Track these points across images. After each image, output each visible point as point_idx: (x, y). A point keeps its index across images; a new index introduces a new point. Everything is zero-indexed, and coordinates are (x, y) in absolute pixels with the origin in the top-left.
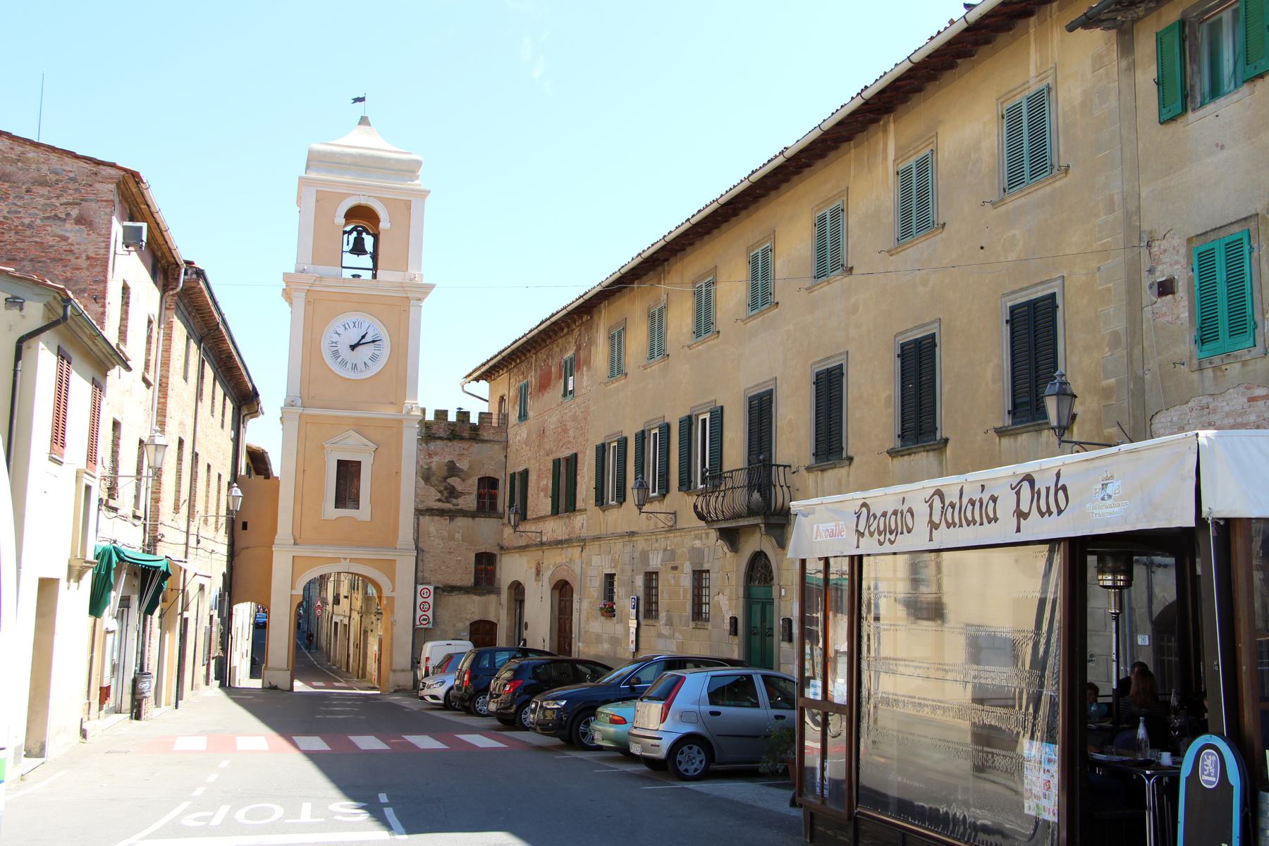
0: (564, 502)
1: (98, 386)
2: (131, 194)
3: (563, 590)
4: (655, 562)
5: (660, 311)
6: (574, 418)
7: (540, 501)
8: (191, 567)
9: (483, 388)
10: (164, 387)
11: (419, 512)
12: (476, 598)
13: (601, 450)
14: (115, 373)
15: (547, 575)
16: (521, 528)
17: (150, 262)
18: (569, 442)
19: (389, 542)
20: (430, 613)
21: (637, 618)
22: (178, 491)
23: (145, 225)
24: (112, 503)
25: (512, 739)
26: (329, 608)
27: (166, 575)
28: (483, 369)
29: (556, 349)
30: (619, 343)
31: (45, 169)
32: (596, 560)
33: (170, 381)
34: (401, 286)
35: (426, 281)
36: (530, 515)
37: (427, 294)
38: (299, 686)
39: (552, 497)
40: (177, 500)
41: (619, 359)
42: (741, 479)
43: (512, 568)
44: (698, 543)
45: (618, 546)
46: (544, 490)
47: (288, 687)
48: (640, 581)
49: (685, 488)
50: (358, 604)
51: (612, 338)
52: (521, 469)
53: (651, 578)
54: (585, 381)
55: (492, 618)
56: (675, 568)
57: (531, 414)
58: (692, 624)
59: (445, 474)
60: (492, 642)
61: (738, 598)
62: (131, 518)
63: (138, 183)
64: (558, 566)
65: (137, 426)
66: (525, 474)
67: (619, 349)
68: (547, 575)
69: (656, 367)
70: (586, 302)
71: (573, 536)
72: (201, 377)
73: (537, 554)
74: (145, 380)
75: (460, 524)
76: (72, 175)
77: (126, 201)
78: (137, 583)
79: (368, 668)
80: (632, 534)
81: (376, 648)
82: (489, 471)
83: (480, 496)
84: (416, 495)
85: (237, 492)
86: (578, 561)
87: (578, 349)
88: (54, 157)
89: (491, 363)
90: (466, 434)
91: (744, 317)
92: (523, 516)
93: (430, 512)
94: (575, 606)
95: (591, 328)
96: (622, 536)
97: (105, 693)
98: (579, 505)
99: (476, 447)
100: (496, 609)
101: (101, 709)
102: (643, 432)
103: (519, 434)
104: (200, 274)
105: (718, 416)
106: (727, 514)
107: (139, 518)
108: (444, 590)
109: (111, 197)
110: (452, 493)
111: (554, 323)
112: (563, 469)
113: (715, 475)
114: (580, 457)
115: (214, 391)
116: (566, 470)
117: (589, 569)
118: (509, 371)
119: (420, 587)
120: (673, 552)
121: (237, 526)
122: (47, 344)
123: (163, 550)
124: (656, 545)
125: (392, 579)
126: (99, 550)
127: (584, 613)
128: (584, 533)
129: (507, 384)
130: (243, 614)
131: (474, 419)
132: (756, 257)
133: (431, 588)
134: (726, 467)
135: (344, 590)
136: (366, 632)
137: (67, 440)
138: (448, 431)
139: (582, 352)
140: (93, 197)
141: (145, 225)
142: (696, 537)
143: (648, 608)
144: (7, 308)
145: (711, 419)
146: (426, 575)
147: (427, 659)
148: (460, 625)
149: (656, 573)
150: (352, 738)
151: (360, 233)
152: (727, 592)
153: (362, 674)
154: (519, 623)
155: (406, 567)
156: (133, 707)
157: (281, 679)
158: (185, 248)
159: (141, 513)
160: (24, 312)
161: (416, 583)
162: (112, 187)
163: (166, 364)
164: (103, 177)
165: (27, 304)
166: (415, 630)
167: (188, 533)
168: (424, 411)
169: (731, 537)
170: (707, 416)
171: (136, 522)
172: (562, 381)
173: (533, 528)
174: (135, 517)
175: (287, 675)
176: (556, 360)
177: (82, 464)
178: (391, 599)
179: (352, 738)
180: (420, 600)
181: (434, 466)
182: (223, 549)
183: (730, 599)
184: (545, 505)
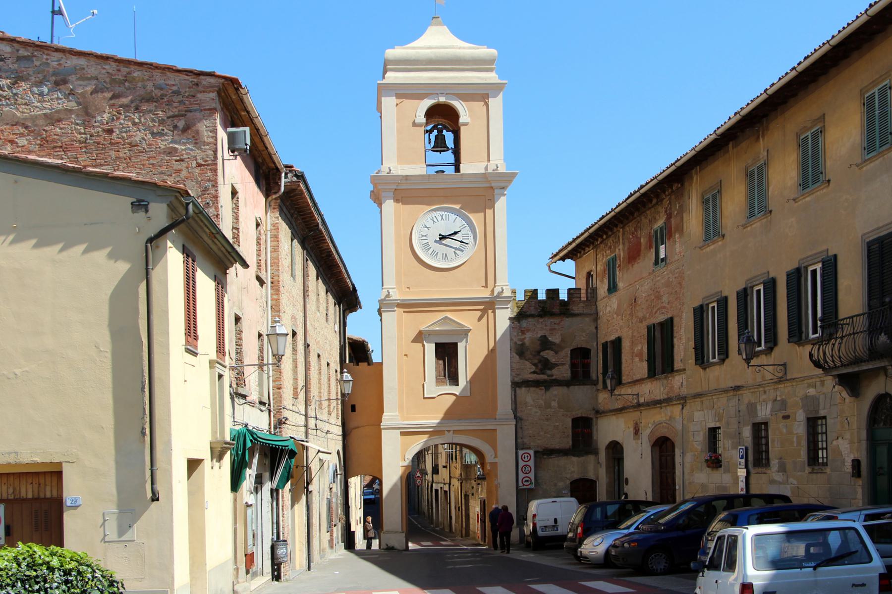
0: (661, 361)
1: (221, 283)
2: (232, 103)
3: (663, 448)
4: (764, 412)
5: (760, 169)
6: (668, 284)
7: (634, 364)
8: (313, 445)
9: (569, 266)
10: (276, 286)
11: (516, 385)
12: (575, 459)
13: (700, 312)
14: (235, 272)
15: (646, 433)
16: (616, 392)
17: (253, 170)
18: (664, 307)
19: (490, 413)
20: (532, 475)
21: (746, 467)
22: (296, 379)
23: (247, 129)
24: (241, 391)
25: (640, 584)
26: (429, 477)
27: (292, 454)
28: (570, 248)
29: (645, 221)
30: (714, 206)
31: (150, 85)
32: (698, 415)
33: (281, 279)
34: (485, 176)
36: (625, 379)
37: (510, 181)
38: (411, 546)
39: (648, 361)
40: (295, 389)
41: (715, 221)
42: (861, 324)
43: (611, 429)
44: (812, 391)
45: (722, 401)
46: (640, 355)
47: (404, 547)
48: (747, 432)
49: (795, 339)
50: (457, 472)
51: (705, 202)
52: (613, 338)
53: (760, 430)
54: (678, 248)
55: (591, 476)
56: (786, 417)
57: (621, 285)
58: (808, 469)
60: (593, 497)
61: (860, 441)
62: (257, 405)
63: (237, 89)
64: (658, 425)
65: (256, 320)
66: (617, 343)
67: (714, 212)
68: (646, 433)
69: (757, 225)
70: (678, 168)
71: (671, 395)
72: (305, 276)
73: (634, 415)
74: (259, 279)
75: (555, 393)
76: (175, 88)
77: (228, 109)
78: (267, 462)
79: (471, 527)
80: (737, 388)
81: (478, 509)
82: (581, 341)
83: (573, 366)
84: (512, 369)
85: (347, 376)
86: (678, 418)
87: (669, 217)
88: (157, 74)
89: (578, 241)
90: (556, 310)
91: (859, 161)
92: (619, 382)
93: (526, 383)
94: (678, 459)
95: (682, 195)
96: (725, 391)
97: (250, 559)
98: (677, 365)
99: (567, 321)
100: (596, 469)
101: (247, 572)
102: (745, 289)
103: (608, 306)
104: (301, 177)
105: (831, 265)
106: (845, 361)
107: (264, 404)
108: (544, 454)
109: (214, 105)
110: (546, 365)
111: (643, 195)
112: (609, 350)
113: (831, 322)
114: (676, 320)
115: (317, 287)
116: (661, 337)
117: (691, 425)
118: (595, 247)
119: (521, 452)
120: (784, 403)
121: (349, 408)
122: (173, 242)
123: (288, 432)
124: (764, 397)
125: (494, 446)
126: (234, 433)
127: (687, 466)
128: (684, 392)
129: (596, 261)
130: (356, 484)
131: (563, 296)
132: (872, 96)
133: (532, 452)
134: (841, 316)
135: (442, 461)
136: (467, 496)
137: (199, 333)
138: (538, 309)
139: (673, 221)
140: (197, 107)
141: (247, 129)
142: (809, 386)
143: (759, 456)
144: (133, 212)
145: (823, 269)
146: (525, 440)
147: (534, 516)
148: (561, 484)
149: (766, 424)
150: (480, 589)
151: (440, 131)
152: (847, 436)
153: (467, 532)
154: (618, 478)
155: (506, 435)
156: (273, 570)
157: (397, 540)
158: (285, 151)
159: (265, 400)
160: (149, 214)
161: (517, 449)
162: (213, 95)
163: (276, 263)
164: (204, 87)
165: (152, 206)
166: (519, 491)
167: (306, 415)
168: (514, 292)
169: (852, 383)
170: (818, 267)
171: (263, 408)
172: (653, 250)
173: (629, 391)
174: (261, 403)
175: (402, 537)
176: (645, 232)
177: (213, 356)
178: (494, 465)
179: (480, 589)
180: (521, 464)
181: (527, 341)
182: (338, 430)
183: (851, 442)
184: (642, 369)
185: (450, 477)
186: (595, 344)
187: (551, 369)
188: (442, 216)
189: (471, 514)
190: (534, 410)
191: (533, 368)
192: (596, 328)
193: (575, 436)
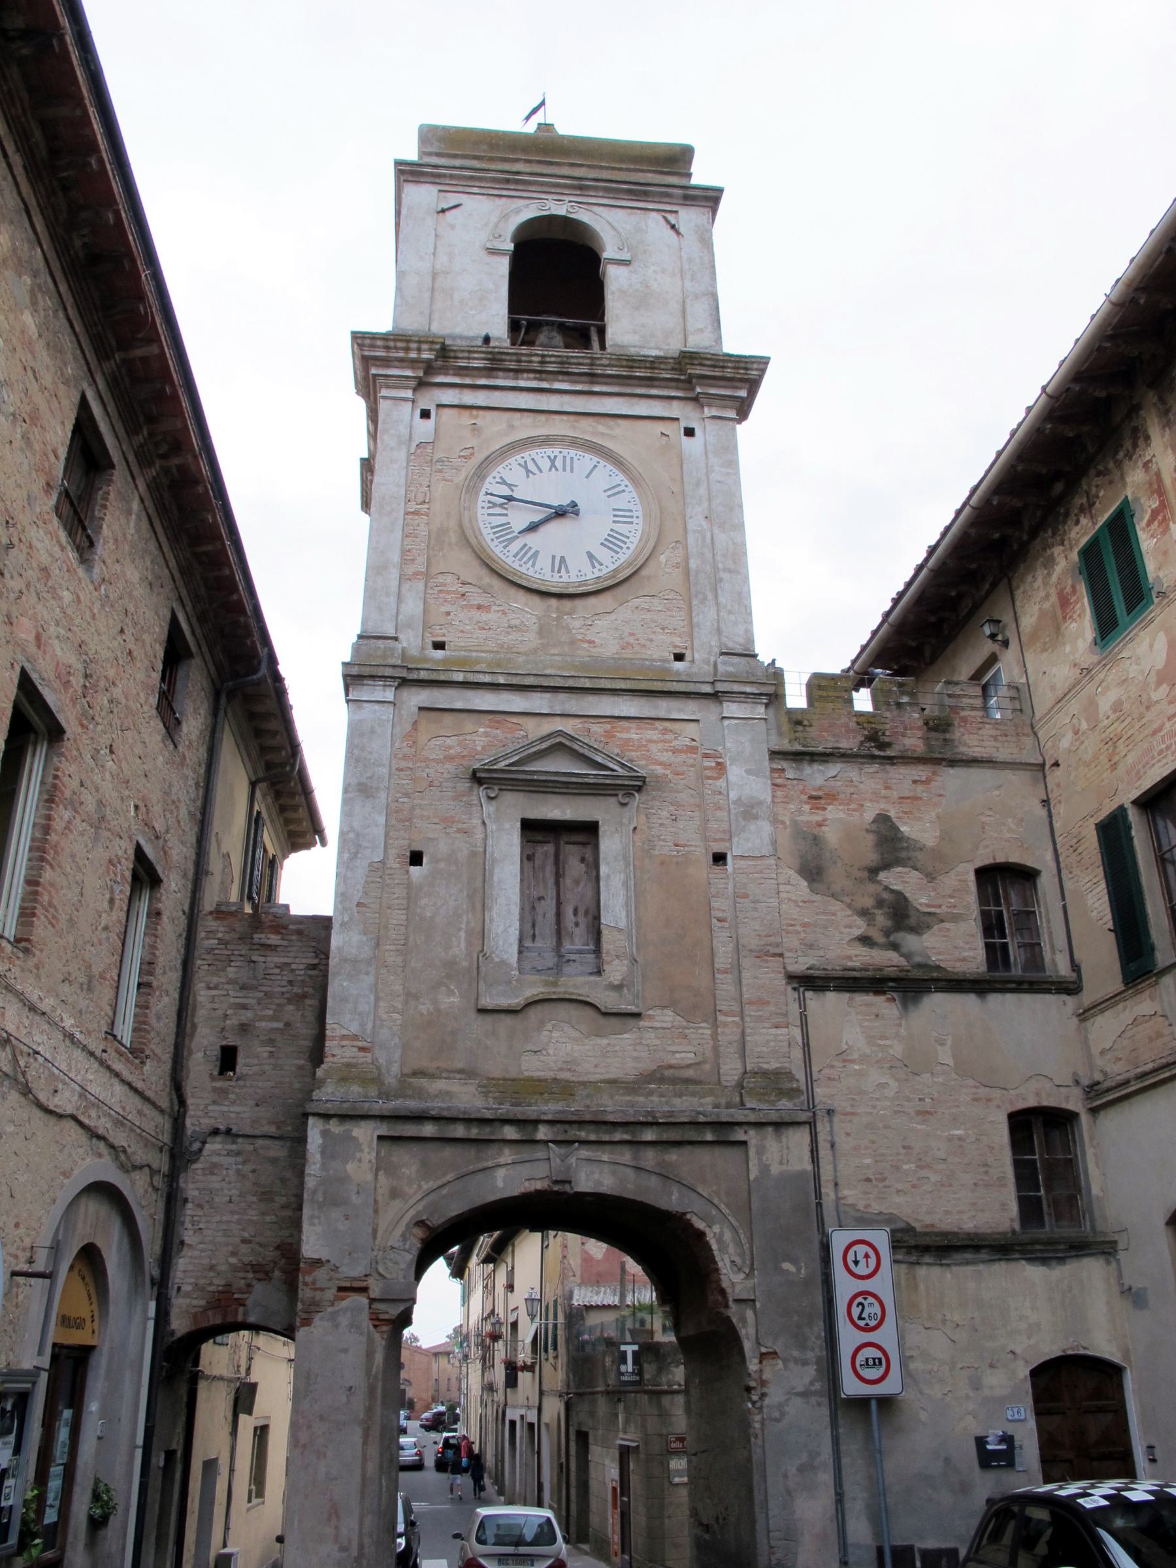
12: (1034, 1273)
35: (733, 344)
59: (871, 857)
99: (951, 779)
110: (901, 915)
136: (583, 1438)
181: (831, 836)
185: (541, 1393)
186: (1049, 856)
187: (916, 930)
188: (553, 461)
189: (594, 1485)
190: (876, 1076)
191: (860, 927)
192: (1046, 802)
193: (1025, 1174)
